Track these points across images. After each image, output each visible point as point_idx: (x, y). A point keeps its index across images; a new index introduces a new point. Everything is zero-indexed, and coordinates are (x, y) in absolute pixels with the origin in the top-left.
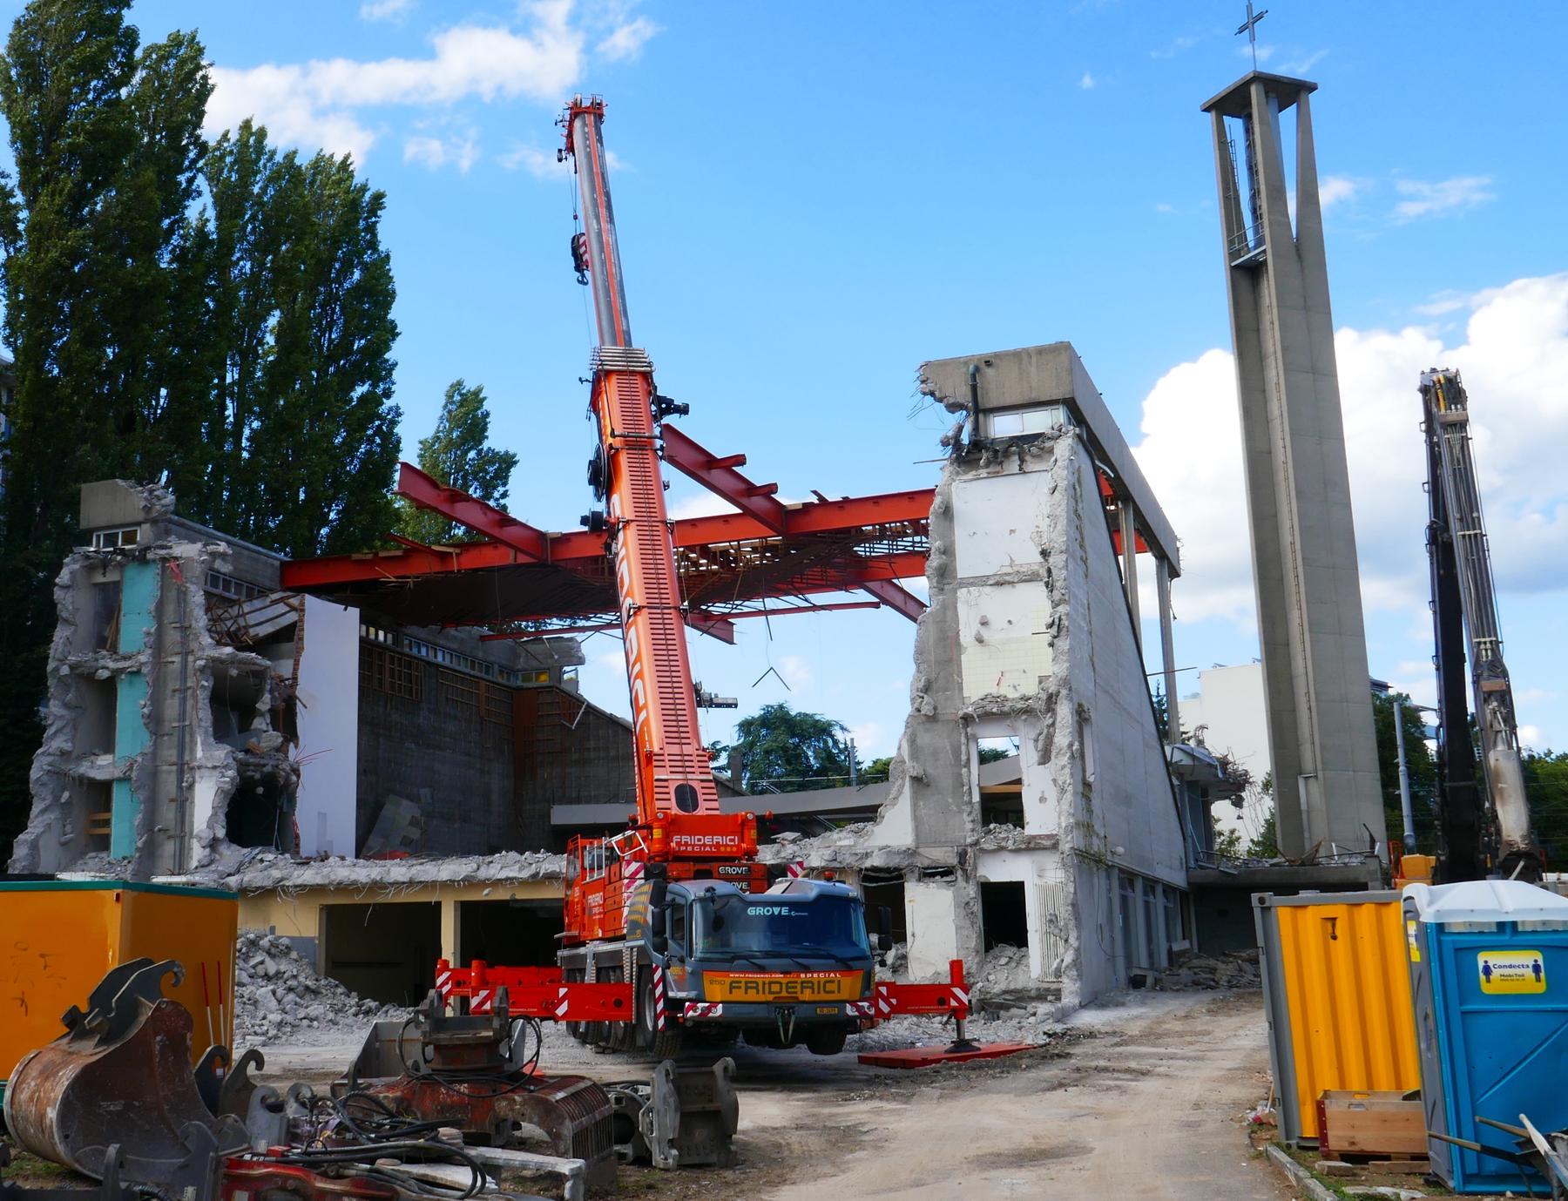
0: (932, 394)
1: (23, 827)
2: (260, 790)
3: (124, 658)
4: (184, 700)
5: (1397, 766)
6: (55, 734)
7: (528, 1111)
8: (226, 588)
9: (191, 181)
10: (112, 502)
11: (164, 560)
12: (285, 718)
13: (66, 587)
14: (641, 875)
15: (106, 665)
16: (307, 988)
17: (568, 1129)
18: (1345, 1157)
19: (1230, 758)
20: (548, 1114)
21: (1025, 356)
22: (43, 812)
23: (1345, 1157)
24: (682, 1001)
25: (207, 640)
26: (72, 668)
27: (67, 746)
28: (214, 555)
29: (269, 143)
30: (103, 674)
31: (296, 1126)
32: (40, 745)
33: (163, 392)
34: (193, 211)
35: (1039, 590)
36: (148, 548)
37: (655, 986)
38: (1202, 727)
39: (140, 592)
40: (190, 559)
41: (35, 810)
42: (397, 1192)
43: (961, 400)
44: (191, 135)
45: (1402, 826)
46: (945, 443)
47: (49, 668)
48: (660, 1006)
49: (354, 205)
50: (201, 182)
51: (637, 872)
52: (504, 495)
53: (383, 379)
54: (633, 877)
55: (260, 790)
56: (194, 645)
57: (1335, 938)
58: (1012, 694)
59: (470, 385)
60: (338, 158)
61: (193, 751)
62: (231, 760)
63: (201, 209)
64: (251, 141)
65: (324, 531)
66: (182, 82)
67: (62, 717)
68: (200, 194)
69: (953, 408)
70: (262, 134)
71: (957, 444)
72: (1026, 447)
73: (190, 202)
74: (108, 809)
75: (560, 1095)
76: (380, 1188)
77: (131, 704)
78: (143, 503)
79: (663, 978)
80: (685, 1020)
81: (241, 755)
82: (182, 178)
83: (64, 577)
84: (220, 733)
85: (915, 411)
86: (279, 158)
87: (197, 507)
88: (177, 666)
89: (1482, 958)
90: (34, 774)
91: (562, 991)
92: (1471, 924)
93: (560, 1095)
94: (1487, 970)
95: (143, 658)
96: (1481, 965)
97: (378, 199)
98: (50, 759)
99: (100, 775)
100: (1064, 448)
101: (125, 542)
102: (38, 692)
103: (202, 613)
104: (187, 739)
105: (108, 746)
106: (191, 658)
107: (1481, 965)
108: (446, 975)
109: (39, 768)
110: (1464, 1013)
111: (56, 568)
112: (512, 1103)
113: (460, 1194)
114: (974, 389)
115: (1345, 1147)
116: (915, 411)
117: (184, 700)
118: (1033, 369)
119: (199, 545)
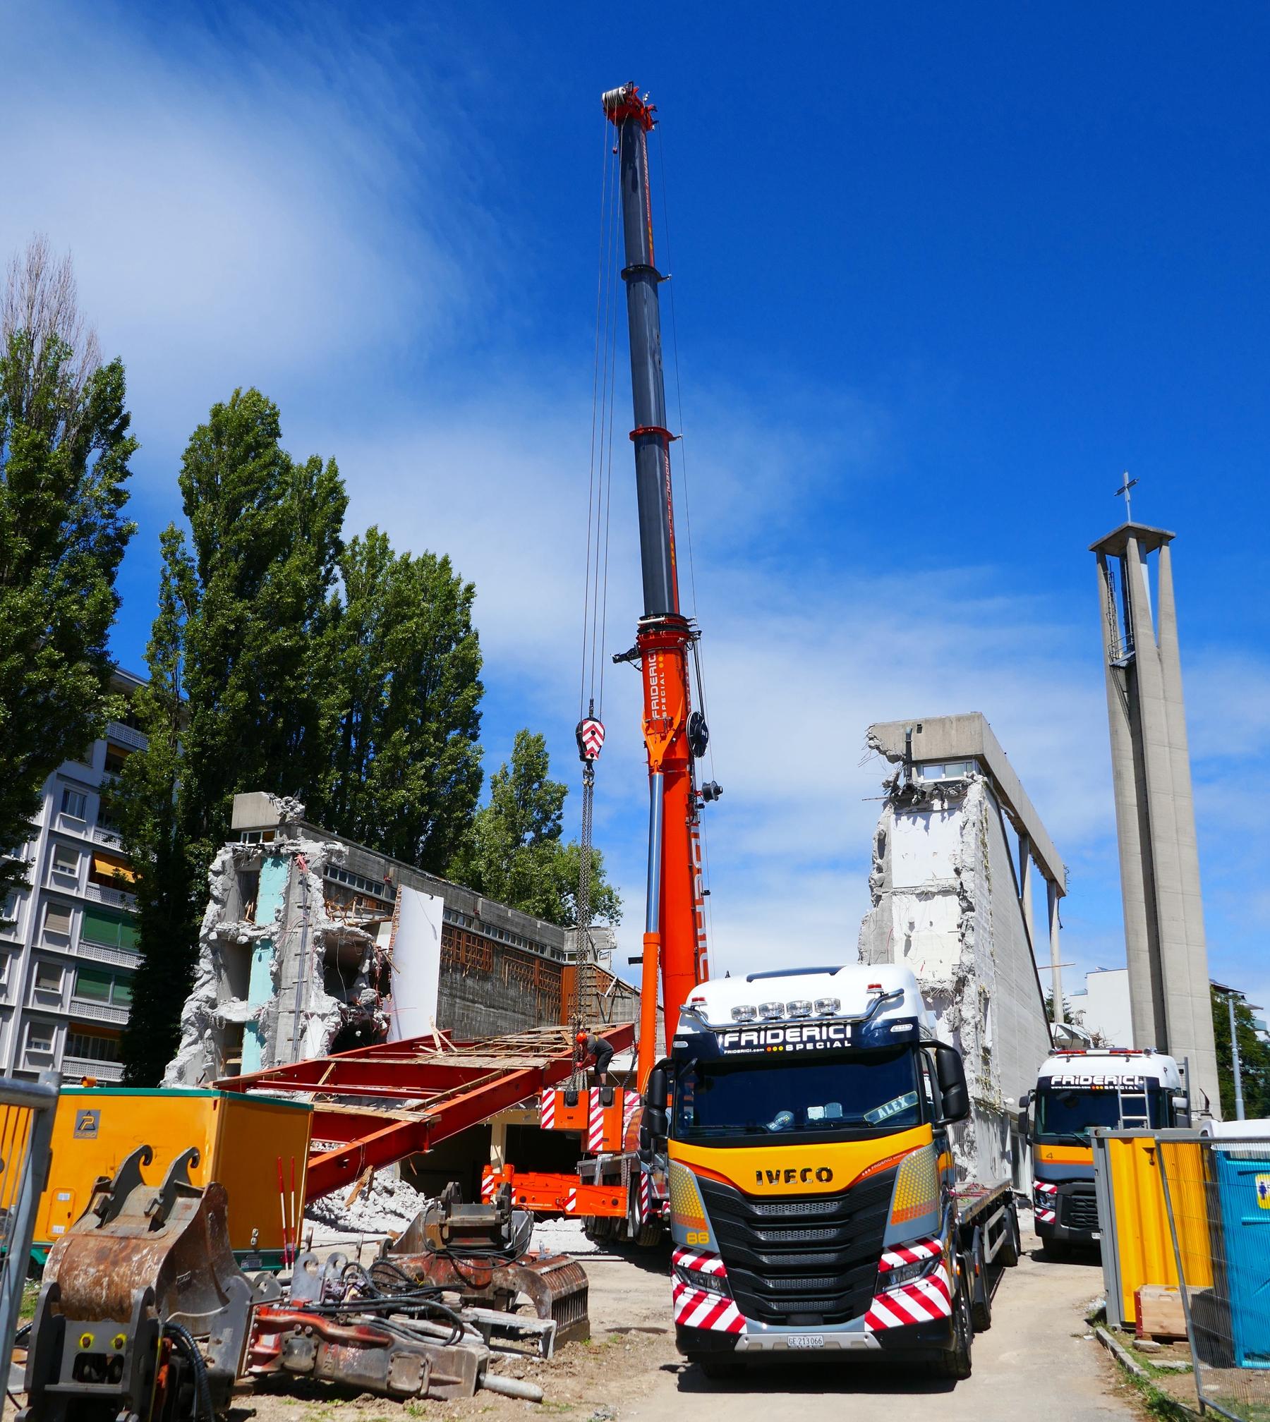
0: (878, 748)
1: (172, 1056)
2: (358, 1033)
3: (259, 929)
4: (302, 962)
5: (1230, 1048)
6: (203, 985)
7: (518, 1281)
8: (378, 892)
9: (329, 571)
10: (254, 809)
11: (294, 854)
12: (382, 981)
13: (217, 873)
14: (638, 1103)
15: (246, 932)
16: (385, 1188)
17: (548, 1297)
18: (1156, 1338)
19: (1101, 1036)
20: (535, 1283)
21: (948, 723)
22: (190, 1045)
23: (1156, 1338)
24: (661, 1201)
25: (322, 915)
26: (219, 934)
27: (213, 995)
28: (331, 852)
29: (391, 546)
30: (244, 939)
31: (329, 1286)
32: (191, 992)
33: (303, 730)
34: (331, 591)
35: (954, 899)
36: (282, 845)
37: (642, 1189)
38: (1081, 1012)
39: (273, 879)
40: (313, 855)
41: (186, 1040)
42: (392, 1339)
43: (899, 753)
44: (331, 537)
45: (1234, 1095)
46: (887, 785)
47: (201, 934)
48: (645, 1205)
49: (451, 595)
50: (337, 571)
51: (634, 1101)
52: (559, 817)
53: (471, 726)
54: (631, 1104)
55: (358, 1033)
56: (312, 920)
57: (750, 979)
58: (930, 979)
59: (533, 735)
60: (439, 559)
61: (307, 1001)
62: (336, 1009)
63: (337, 591)
64: (378, 546)
65: (422, 838)
66: (326, 498)
67: (209, 972)
68: (336, 580)
69: (893, 759)
70: (385, 539)
71: (895, 788)
72: (953, 795)
73: (329, 586)
74: (1247, 1118)
75: (546, 1269)
76: (379, 1335)
77: (261, 968)
78: (281, 811)
79: (649, 1182)
80: (663, 1215)
81: (344, 1006)
82: (323, 569)
83: (216, 865)
84: (331, 988)
85: (865, 760)
86: (397, 558)
87: (320, 818)
88: (300, 936)
89: (1259, 1180)
90: (185, 1014)
91: (572, 1191)
92: (1250, 1153)
93: (546, 1269)
94: (1263, 1190)
95: (274, 929)
96: (1258, 1184)
97: (469, 589)
98: (198, 1004)
99: (236, 1018)
100: (976, 792)
101: (266, 840)
102: (195, 957)
103: (321, 895)
104: (304, 991)
105: (243, 994)
106: (310, 930)
107: (1258, 1184)
108: (491, 1177)
109: (189, 1010)
110: (1245, 1223)
111: (211, 858)
112: (506, 1276)
113: (443, 1341)
114: (908, 744)
115: (1157, 1330)
116: (865, 760)
117: (302, 962)
118: (953, 732)
119: (321, 844)
